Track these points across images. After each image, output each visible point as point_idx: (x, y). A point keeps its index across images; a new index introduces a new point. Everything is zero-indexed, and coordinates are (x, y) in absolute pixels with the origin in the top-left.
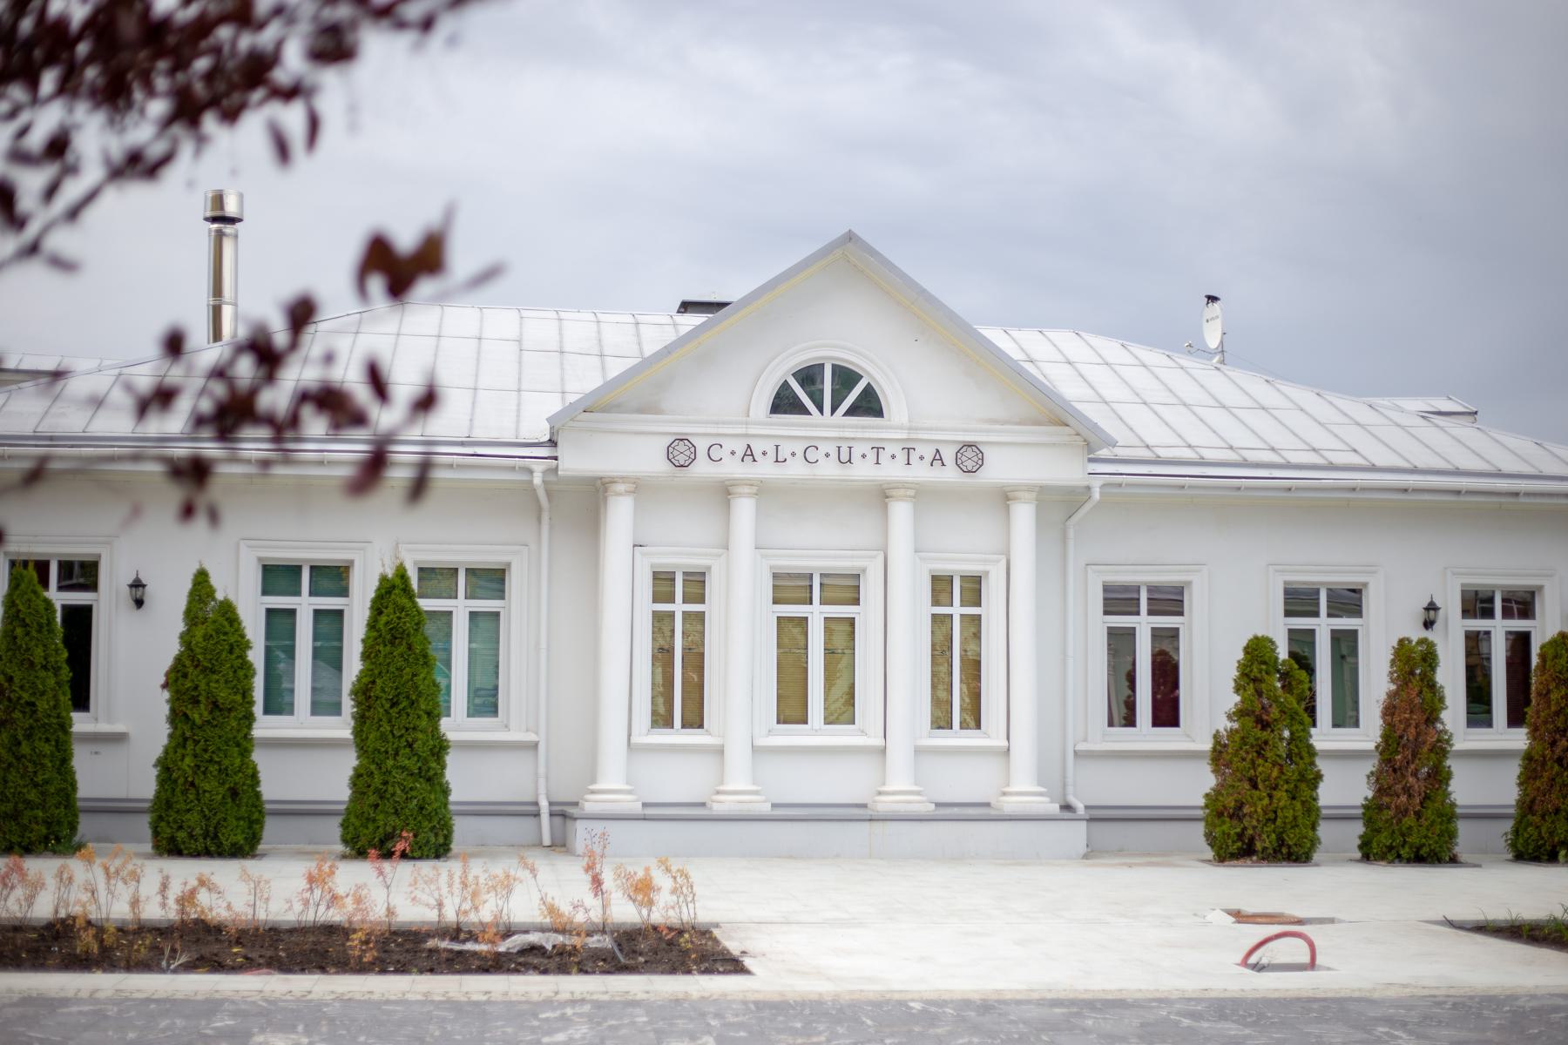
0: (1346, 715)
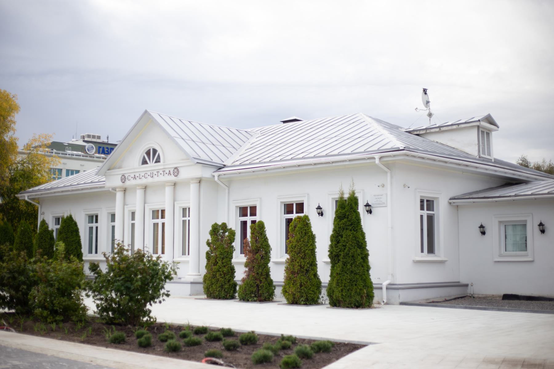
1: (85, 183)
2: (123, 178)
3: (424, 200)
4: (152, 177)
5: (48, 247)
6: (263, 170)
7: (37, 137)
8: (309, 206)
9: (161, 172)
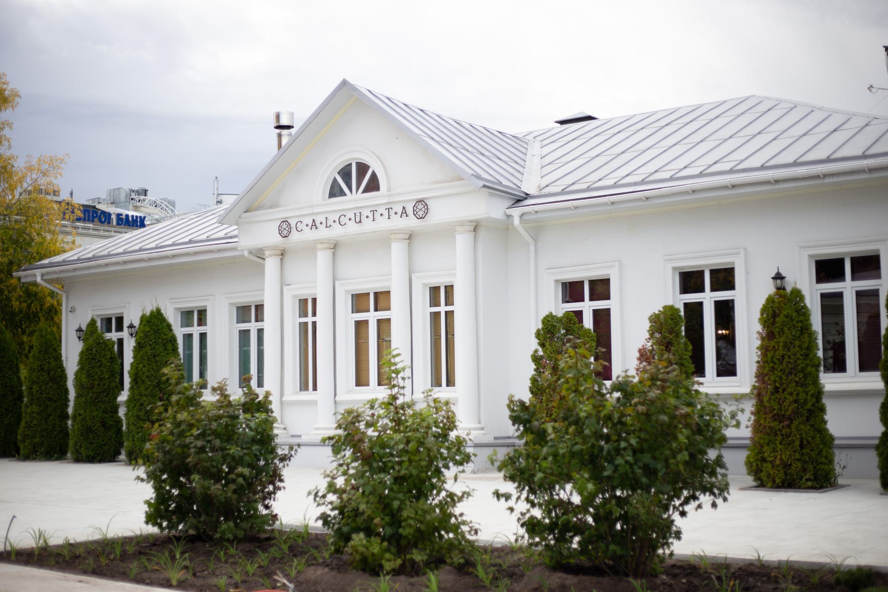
0: (727, 368)
1: (173, 245)
2: (284, 226)
3: (300, 323)
4: (360, 222)
5: (107, 376)
6: (640, 200)
7: (34, 162)
8: (748, 273)
9: (382, 210)
